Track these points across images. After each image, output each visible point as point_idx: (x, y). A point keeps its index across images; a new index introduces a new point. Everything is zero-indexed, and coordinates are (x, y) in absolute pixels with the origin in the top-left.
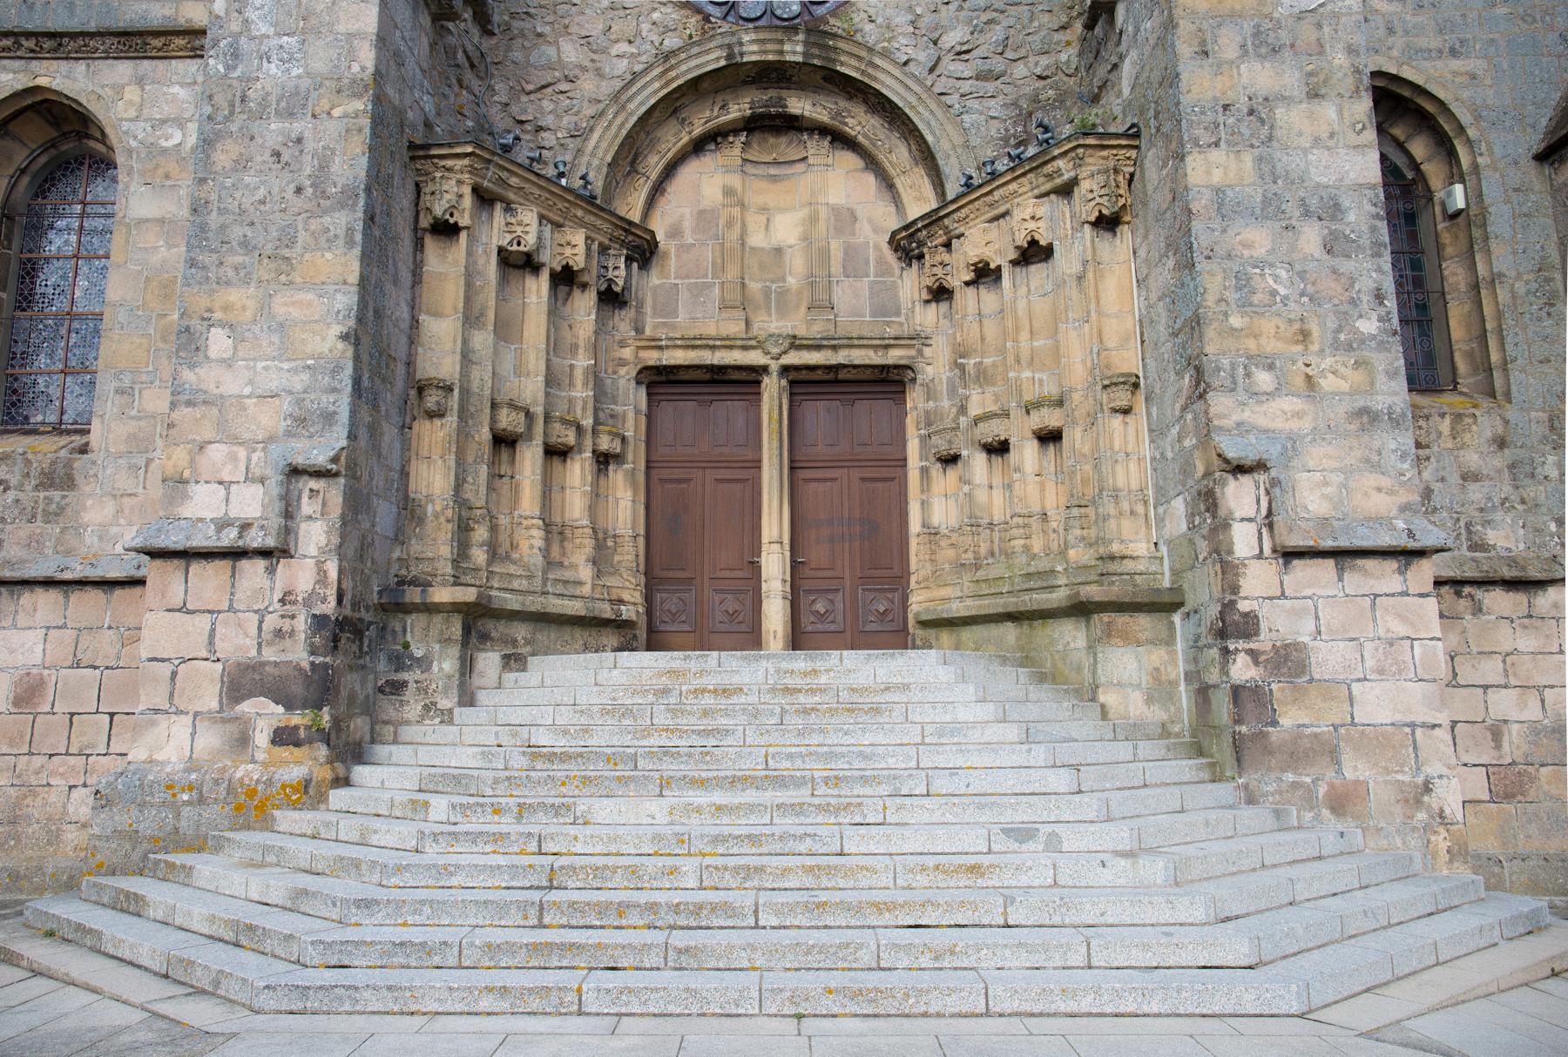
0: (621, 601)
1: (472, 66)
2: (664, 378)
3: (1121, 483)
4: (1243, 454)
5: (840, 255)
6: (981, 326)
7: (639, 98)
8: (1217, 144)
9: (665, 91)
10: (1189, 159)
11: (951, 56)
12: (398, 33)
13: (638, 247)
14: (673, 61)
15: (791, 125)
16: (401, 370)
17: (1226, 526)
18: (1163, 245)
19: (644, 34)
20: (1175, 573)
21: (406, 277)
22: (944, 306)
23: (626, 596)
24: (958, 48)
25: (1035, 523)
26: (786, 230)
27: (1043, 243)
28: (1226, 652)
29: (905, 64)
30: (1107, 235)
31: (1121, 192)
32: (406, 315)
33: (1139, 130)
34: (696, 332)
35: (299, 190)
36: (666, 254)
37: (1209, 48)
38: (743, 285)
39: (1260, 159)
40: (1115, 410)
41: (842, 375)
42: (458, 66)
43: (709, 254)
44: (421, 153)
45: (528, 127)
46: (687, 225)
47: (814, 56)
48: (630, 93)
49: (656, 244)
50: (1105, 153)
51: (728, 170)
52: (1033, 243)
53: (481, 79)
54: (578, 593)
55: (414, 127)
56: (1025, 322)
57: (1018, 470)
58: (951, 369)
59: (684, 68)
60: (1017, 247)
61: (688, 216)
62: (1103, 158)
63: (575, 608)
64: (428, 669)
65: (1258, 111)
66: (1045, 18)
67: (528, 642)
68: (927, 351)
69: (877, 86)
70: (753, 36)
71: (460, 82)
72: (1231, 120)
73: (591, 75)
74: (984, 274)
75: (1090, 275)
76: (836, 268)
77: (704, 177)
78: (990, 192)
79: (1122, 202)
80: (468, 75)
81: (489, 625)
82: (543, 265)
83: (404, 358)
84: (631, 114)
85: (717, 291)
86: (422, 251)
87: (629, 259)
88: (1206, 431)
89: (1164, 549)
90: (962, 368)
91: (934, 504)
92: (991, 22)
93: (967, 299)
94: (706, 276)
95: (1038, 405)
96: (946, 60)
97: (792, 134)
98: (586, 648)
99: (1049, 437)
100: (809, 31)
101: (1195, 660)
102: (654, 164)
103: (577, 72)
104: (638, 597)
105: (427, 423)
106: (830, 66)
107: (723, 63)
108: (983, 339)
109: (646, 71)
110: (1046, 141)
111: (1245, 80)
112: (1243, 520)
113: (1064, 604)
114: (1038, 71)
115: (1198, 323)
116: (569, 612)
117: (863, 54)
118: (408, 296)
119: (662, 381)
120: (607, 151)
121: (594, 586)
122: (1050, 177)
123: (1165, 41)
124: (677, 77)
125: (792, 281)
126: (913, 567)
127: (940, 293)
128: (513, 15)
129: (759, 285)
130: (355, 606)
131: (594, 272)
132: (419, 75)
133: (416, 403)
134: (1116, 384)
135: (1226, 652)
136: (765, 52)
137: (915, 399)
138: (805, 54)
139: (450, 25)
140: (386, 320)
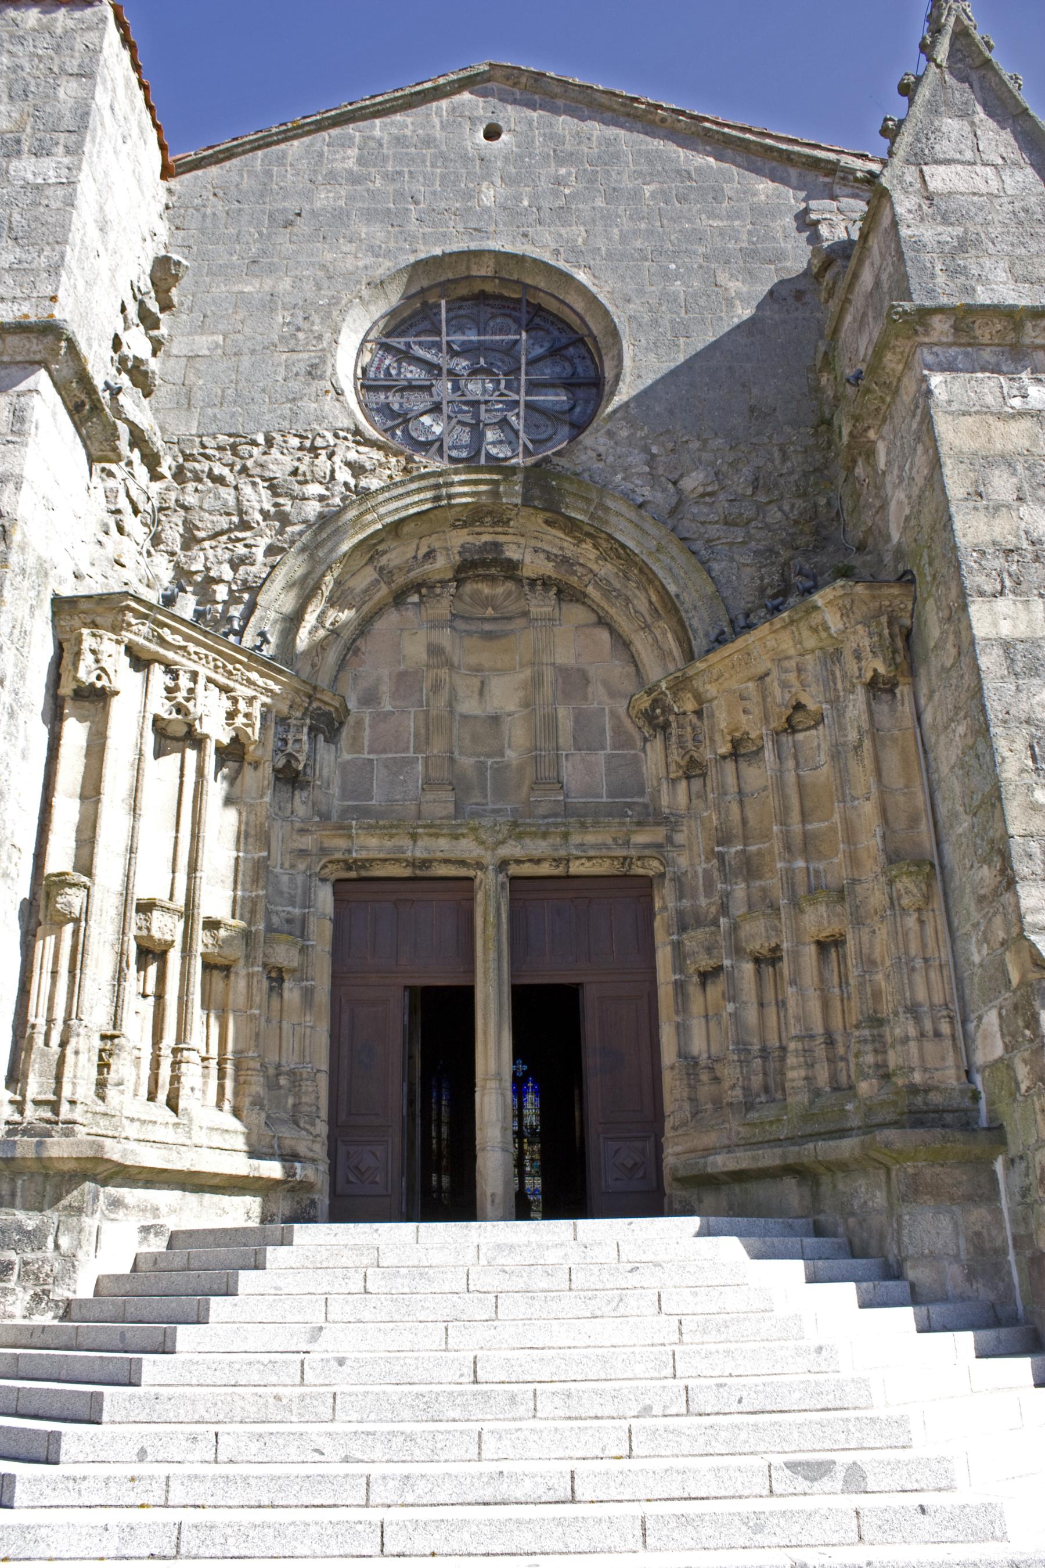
1: (136, 511)
2: (353, 874)
3: (921, 995)
8: (1001, 593)
26: (504, 695)
37: (982, 489)
38: (452, 760)
46: (385, 689)
49: (347, 711)
51: (435, 625)
54: (122, 1068)
58: (708, 860)
59: (382, 510)
71: (121, 530)
76: (565, 738)
82: (207, 736)
85: (420, 768)
90: (721, 857)
101: (1025, 1220)
104: (320, 1150)
107: (428, 506)
108: (744, 822)
129: (472, 760)
139: (113, 467)
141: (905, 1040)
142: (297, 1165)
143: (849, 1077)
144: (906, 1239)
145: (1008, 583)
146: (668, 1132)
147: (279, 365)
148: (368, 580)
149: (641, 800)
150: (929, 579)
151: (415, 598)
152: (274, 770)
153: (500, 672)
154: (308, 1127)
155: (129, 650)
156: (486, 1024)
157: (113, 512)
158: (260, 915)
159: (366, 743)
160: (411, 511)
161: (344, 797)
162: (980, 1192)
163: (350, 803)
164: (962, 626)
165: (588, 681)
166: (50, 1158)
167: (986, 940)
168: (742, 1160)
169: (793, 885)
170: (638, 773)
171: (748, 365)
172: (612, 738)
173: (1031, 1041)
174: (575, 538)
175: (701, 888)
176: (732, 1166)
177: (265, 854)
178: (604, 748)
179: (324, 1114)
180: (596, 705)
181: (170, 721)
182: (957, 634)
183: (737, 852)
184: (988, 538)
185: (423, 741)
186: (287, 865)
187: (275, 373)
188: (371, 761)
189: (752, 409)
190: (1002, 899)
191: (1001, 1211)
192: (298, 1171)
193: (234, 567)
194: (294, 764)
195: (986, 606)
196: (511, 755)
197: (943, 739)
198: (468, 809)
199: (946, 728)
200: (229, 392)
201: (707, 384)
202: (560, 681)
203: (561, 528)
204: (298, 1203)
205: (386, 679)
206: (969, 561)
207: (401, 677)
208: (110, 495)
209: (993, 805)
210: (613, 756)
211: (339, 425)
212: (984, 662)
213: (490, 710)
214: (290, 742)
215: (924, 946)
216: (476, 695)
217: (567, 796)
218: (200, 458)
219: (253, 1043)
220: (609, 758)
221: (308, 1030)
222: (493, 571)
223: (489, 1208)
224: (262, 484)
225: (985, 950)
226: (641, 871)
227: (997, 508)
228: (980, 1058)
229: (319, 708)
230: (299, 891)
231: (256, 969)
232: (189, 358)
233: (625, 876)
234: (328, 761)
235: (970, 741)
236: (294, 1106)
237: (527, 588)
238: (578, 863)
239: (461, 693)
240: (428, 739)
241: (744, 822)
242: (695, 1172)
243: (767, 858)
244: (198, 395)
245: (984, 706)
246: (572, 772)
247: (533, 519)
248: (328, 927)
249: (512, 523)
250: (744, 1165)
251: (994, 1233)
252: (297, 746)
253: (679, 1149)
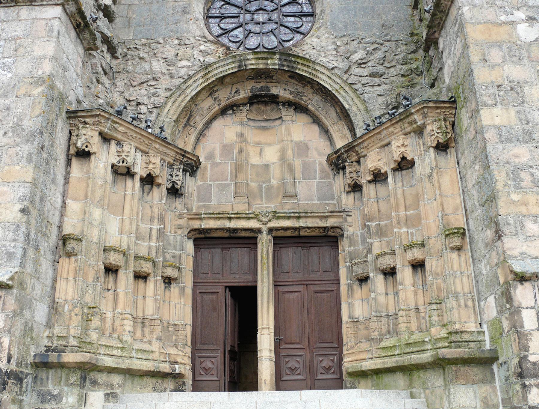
0: (176, 363)
1: (106, 73)
2: (203, 236)
3: (459, 289)
5: (301, 167)
7: (192, 88)
9: (206, 84)
10: (482, 112)
11: (356, 65)
12: (64, 56)
13: (189, 164)
14: (210, 69)
15: (273, 100)
17: (519, 312)
19: (195, 56)
20: (492, 339)
21: (60, 179)
22: (357, 195)
23: (179, 360)
24: (360, 61)
25: (412, 313)
26: (271, 155)
28: (524, 386)
29: (332, 69)
30: (443, 153)
33: (455, 99)
34: (220, 210)
36: (205, 168)
37: (486, 57)
38: (247, 184)
39: (518, 112)
40: (453, 249)
41: (303, 233)
42: (97, 73)
43: (229, 168)
44: (72, 115)
46: (217, 152)
48: (187, 85)
50: (438, 111)
51: (239, 124)
52: (404, 158)
53: (110, 79)
54: (150, 357)
55: (70, 103)
56: (402, 202)
57: (401, 284)
58: (363, 229)
59: (215, 72)
60: (395, 161)
61: (217, 148)
62: (438, 113)
63: (148, 366)
64: (61, 400)
65: (516, 87)
66: (404, 47)
67: (120, 386)
68: (349, 219)
69: (318, 80)
71: (98, 81)
72: (501, 93)
73: (167, 77)
74: (378, 177)
75: (435, 175)
76: (298, 174)
78: (379, 133)
80: (103, 78)
81: (93, 375)
82: (136, 173)
83: (57, 223)
84: (187, 96)
87: (184, 171)
89: (485, 327)
90: (368, 227)
91: (355, 306)
92: (375, 49)
93: (369, 190)
94: (227, 180)
95: (410, 247)
96: (354, 67)
97: (274, 106)
98: (155, 389)
100: (281, 54)
101: (507, 392)
102: (199, 122)
103: (160, 75)
104: (188, 361)
105: (67, 260)
106: (293, 70)
107: (236, 70)
108: (379, 211)
110: (408, 106)
111: (506, 74)
112: (527, 308)
114: (402, 72)
115: (494, 198)
116: (145, 368)
117: (311, 65)
118: (61, 190)
119: (203, 239)
120: (173, 115)
122: (410, 123)
123: (465, 55)
125: (274, 182)
126: (344, 341)
127: (356, 188)
128: (128, 49)
129: (256, 184)
130: (19, 364)
131: (165, 178)
132: (75, 76)
133: (61, 248)
134: (453, 234)
135: (524, 386)
136: (258, 64)
137: (344, 247)
138: (280, 65)
139: (94, 53)
142: (177, 366)
143: (427, 326)
144: (452, 400)
146: (345, 352)
147: (170, 7)
148: (209, 105)
149: (333, 202)
150: (462, 99)
151: (231, 112)
152: (167, 188)
153: (269, 144)
154: (182, 349)
156: (262, 304)
157: (94, 73)
158: (160, 253)
159: (209, 177)
160: (229, 72)
162: (486, 379)
163: (201, 204)
165: (309, 149)
166: (64, 362)
168: (378, 364)
169: (401, 239)
170: (332, 189)
171: (381, 6)
173: (509, 309)
174: (302, 84)
175: (360, 242)
176: (373, 367)
177: (163, 226)
178: (316, 179)
179: (189, 343)
180: (312, 159)
182: (475, 124)
183: (376, 225)
184: (489, 80)
185: (234, 176)
186: (173, 231)
188: (211, 185)
190: (496, 244)
191: (496, 387)
192: (177, 369)
193: (149, 98)
194: (176, 186)
195: (489, 110)
196: (274, 182)
197: (469, 172)
199: (470, 167)
200: (147, 20)
201: (362, 14)
202: (296, 148)
203: (296, 80)
204: (177, 383)
206: (480, 90)
207: (225, 147)
208: (93, 66)
209: (492, 201)
211: (196, 34)
214: (174, 176)
215: (460, 266)
216: (258, 155)
218: (134, 49)
221: (182, 306)
222: (266, 99)
223: (263, 386)
225: (488, 268)
226: (333, 234)
227: (494, 66)
228: (486, 318)
229: (188, 161)
230: (178, 243)
231: (158, 278)
235: (481, 172)
236: (176, 340)
238: (304, 230)
240: (236, 175)
241: (379, 211)
242: (356, 370)
243: (390, 228)
244: (133, 21)
247: (283, 75)
249: (274, 77)
250: (379, 366)
251: (493, 397)
252: (177, 178)
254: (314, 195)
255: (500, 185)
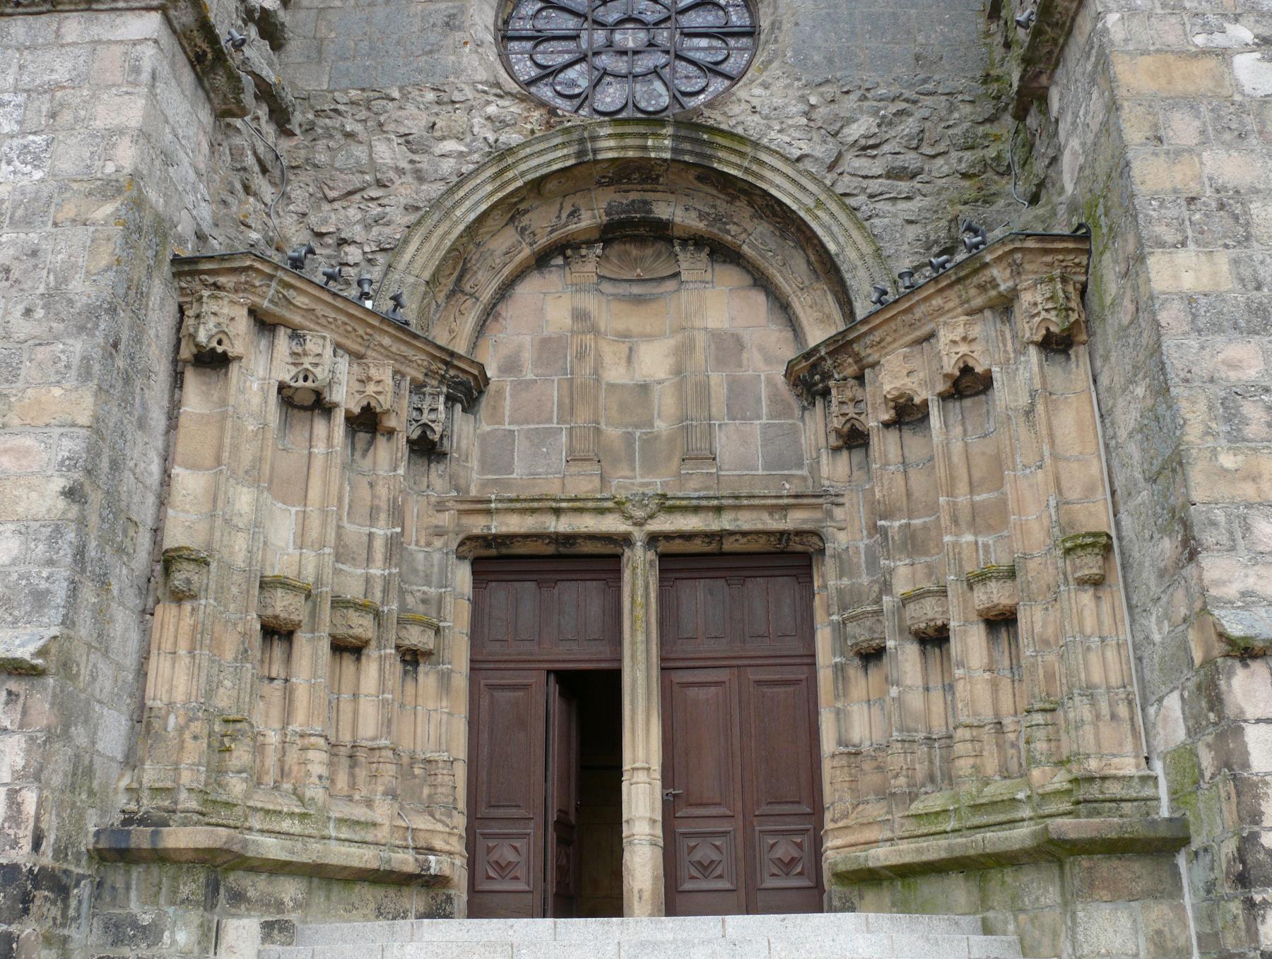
0: (431, 850)
1: (264, 171)
2: (493, 552)
3: (1097, 677)
4: (1251, 633)
6: (906, 478)
7: (468, 204)
8: (1184, 244)
9: (500, 195)
10: (1151, 261)
11: (854, 152)
13: (461, 383)
14: (510, 160)
16: (144, 539)
18: (1129, 367)
19: (476, 130)
21: (158, 419)
22: (858, 455)
23: (438, 843)
24: (863, 142)
25: (987, 735)
26: (654, 362)
27: (979, 370)
28: (1250, 904)
29: (799, 160)
30: (1061, 358)
31: (1073, 305)
32: (155, 468)
33: (1089, 231)
35: (28, 312)
36: (500, 392)
37: (1162, 133)
38: (598, 431)
39: (1236, 262)
41: (729, 546)
42: (245, 169)
44: (186, 268)
45: (329, 240)
46: (527, 356)
47: (684, 152)
48: (457, 197)
49: (487, 381)
50: (1049, 259)
51: (579, 289)
52: (967, 370)
54: (370, 838)
55: (182, 241)
56: (962, 472)
57: (961, 664)
58: (870, 536)
59: (523, 167)
60: (946, 376)
61: (528, 346)
62: (1047, 264)
63: (364, 857)
64: (158, 939)
66: (967, 109)
67: (298, 905)
68: (838, 513)
69: (764, 186)
70: (608, 130)
71: (247, 189)
73: (409, 178)
74: (907, 415)
75: (1040, 408)
77: (548, 298)
78: (909, 310)
79: (1074, 317)
80: (259, 182)
81: (235, 879)
82: (336, 405)
83: (150, 522)
84: (456, 223)
85: (564, 438)
86: (181, 387)
88: (1202, 613)
89: (1158, 767)
90: (884, 532)
91: (852, 718)
93: (886, 445)
94: (550, 420)
95: (982, 577)
96: (848, 156)
97: (660, 246)
98: (380, 913)
99: (1001, 623)
100: (678, 124)
101: (1211, 918)
102: (485, 284)
103: (391, 174)
104: (458, 846)
105: (173, 609)
106: (706, 162)
108: (909, 494)
109: (476, 172)
110: (976, 246)
112: (1258, 721)
113: (1029, 843)
114: (963, 167)
115: (1181, 464)
116: (356, 863)
118: (160, 444)
119: (493, 560)
120: (424, 267)
121: (395, 828)
122: (982, 288)
124: (514, 179)
125: (661, 426)
126: (827, 799)
129: (620, 431)
130: (60, 853)
131: (404, 415)
132: (192, 176)
134: (1083, 547)
135: (1250, 904)
136: (624, 148)
137: (828, 579)
138: (674, 150)
139: (238, 123)
140: (127, 473)
141: (1079, 725)
142: (432, 858)
143: (1021, 765)
144: (1081, 938)
145: (1190, 233)
146: (829, 825)
148: (508, 244)
149: (799, 472)
150: (1105, 230)
151: (559, 261)
153: (650, 337)
154: (443, 818)
155: (252, 312)
156: (633, 711)
158: (394, 594)
159: (507, 413)
160: (555, 167)
161: (484, 468)
162: (1160, 888)
163: (490, 477)
164: (1140, 281)
167: (1167, 616)
168: (905, 853)
169: (961, 560)
170: (797, 442)
171: (913, 12)
172: (768, 406)
173: (1215, 724)
174: (728, 194)
175: (864, 566)
177: (398, 530)
178: (759, 418)
179: (462, 805)
181: (297, 389)
182: (1135, 288)
183: (901, 526)
184: (1168, 186)
185: (567, 410)
186: (422, 542)
187: (411, 24)
189: (917, 58)
190: (1184, 572)
191: (1184, 909)
192: (433, 864)
193: (368, 227)
194: (430, 435)
195: (1167, 258)
196: (661, 426)
197: (1121, 403)
198: (615, 483)
200: (362, 44)
201: (869, 32)
202: (713, 347)
203: (713, 185)
204: (433, 898)
205: (528, 346)
208: (236, 154)
209: (1174, 470)
210: (770, 425)
211: (478, 78)
212: (1163, 317)
213: (639, 378)
214: (426, 412)
215: (1100, 623)
216: (623, 362)
217: (720, 469)
218: (332, 114)
219: (385, 729)
220: (765, 427)
221: (445, 717)
222: (642, 231)
224: (396, 140)
225: (1166, 628)
226: (799, 548)
228: (1160, 744)
230: (436, 569)
231: (388, 651)
232: (321, 10)
233: (783, 553)
234: (465, 432)
235: (1149, 402)
236: (430, 796)
237: (677, 248)
238: (732, 539)
239: (608, 359)
240: (572, 409)
241: (909, 494)
242: (855, 867)
243: (933, 533)
245: (1163, 363)
246: (727, 442)
248: (465, 610)
249: (661, 180)
250: (908, 859)
251: (1176, 931)
252: (433, 417)
253: (839, 842)
254: (755, 456)
255: (1193, 434)
